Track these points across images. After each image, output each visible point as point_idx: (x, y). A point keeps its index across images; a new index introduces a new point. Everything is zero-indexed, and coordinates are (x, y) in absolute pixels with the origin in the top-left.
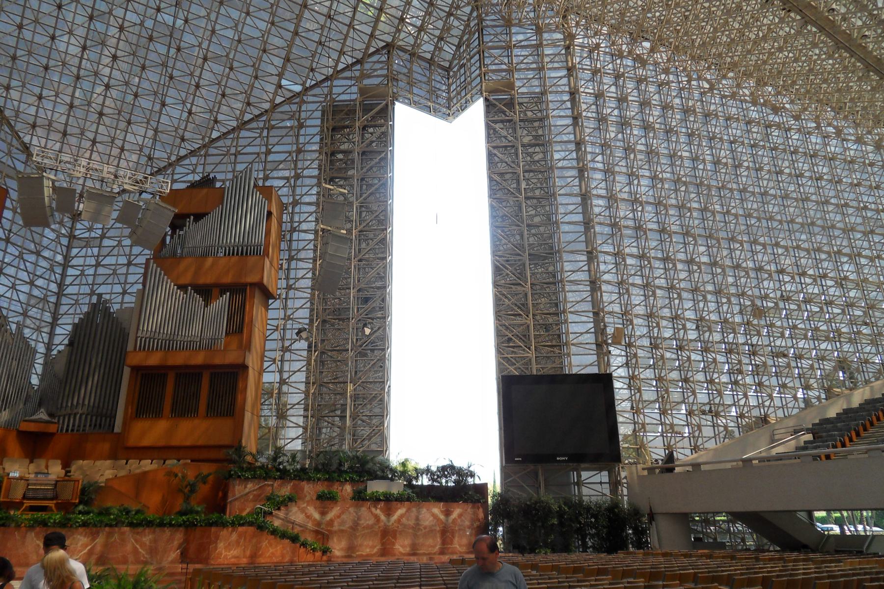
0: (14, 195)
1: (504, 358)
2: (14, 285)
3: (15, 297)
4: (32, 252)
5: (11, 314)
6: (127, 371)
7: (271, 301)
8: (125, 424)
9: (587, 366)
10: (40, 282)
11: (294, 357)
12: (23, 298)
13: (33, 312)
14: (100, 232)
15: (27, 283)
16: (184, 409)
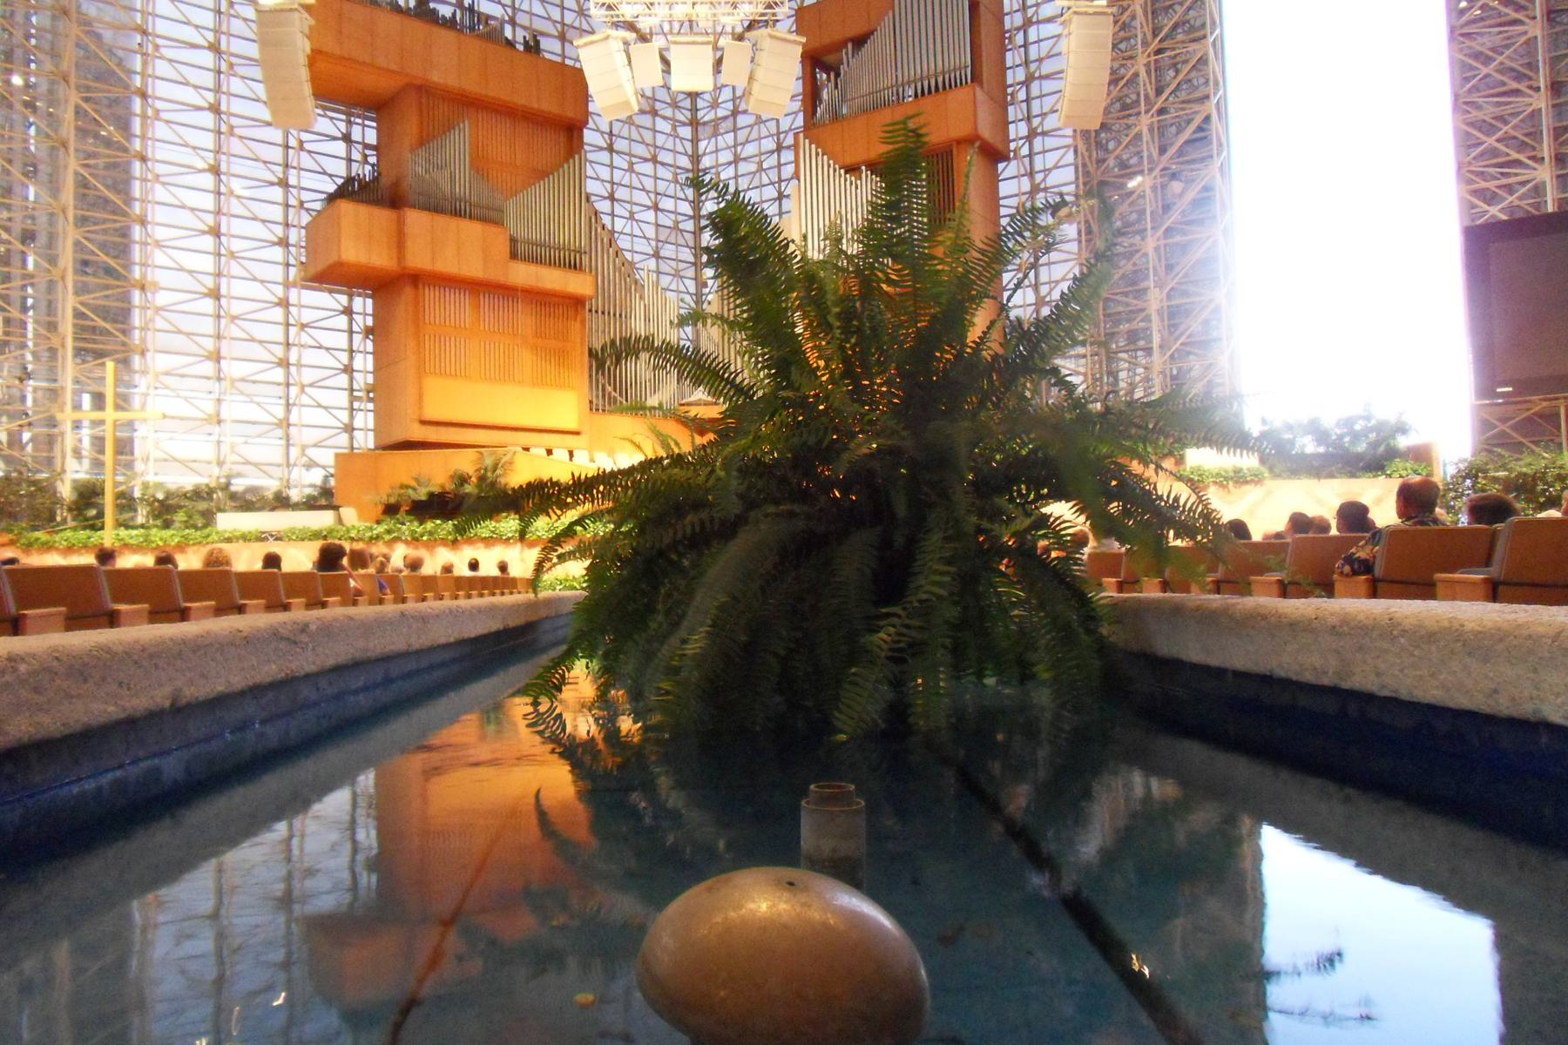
1: (1475, 192)
2: (632, 214)
3: (637, 232)
4: (646, 160)
5: (637, 258)
7: (1001, 166)
9: (248, 463)
10: (666, 204)
12: (650, 232)
13: (668, 251)
14: (730, 106)
15: (649, 208)
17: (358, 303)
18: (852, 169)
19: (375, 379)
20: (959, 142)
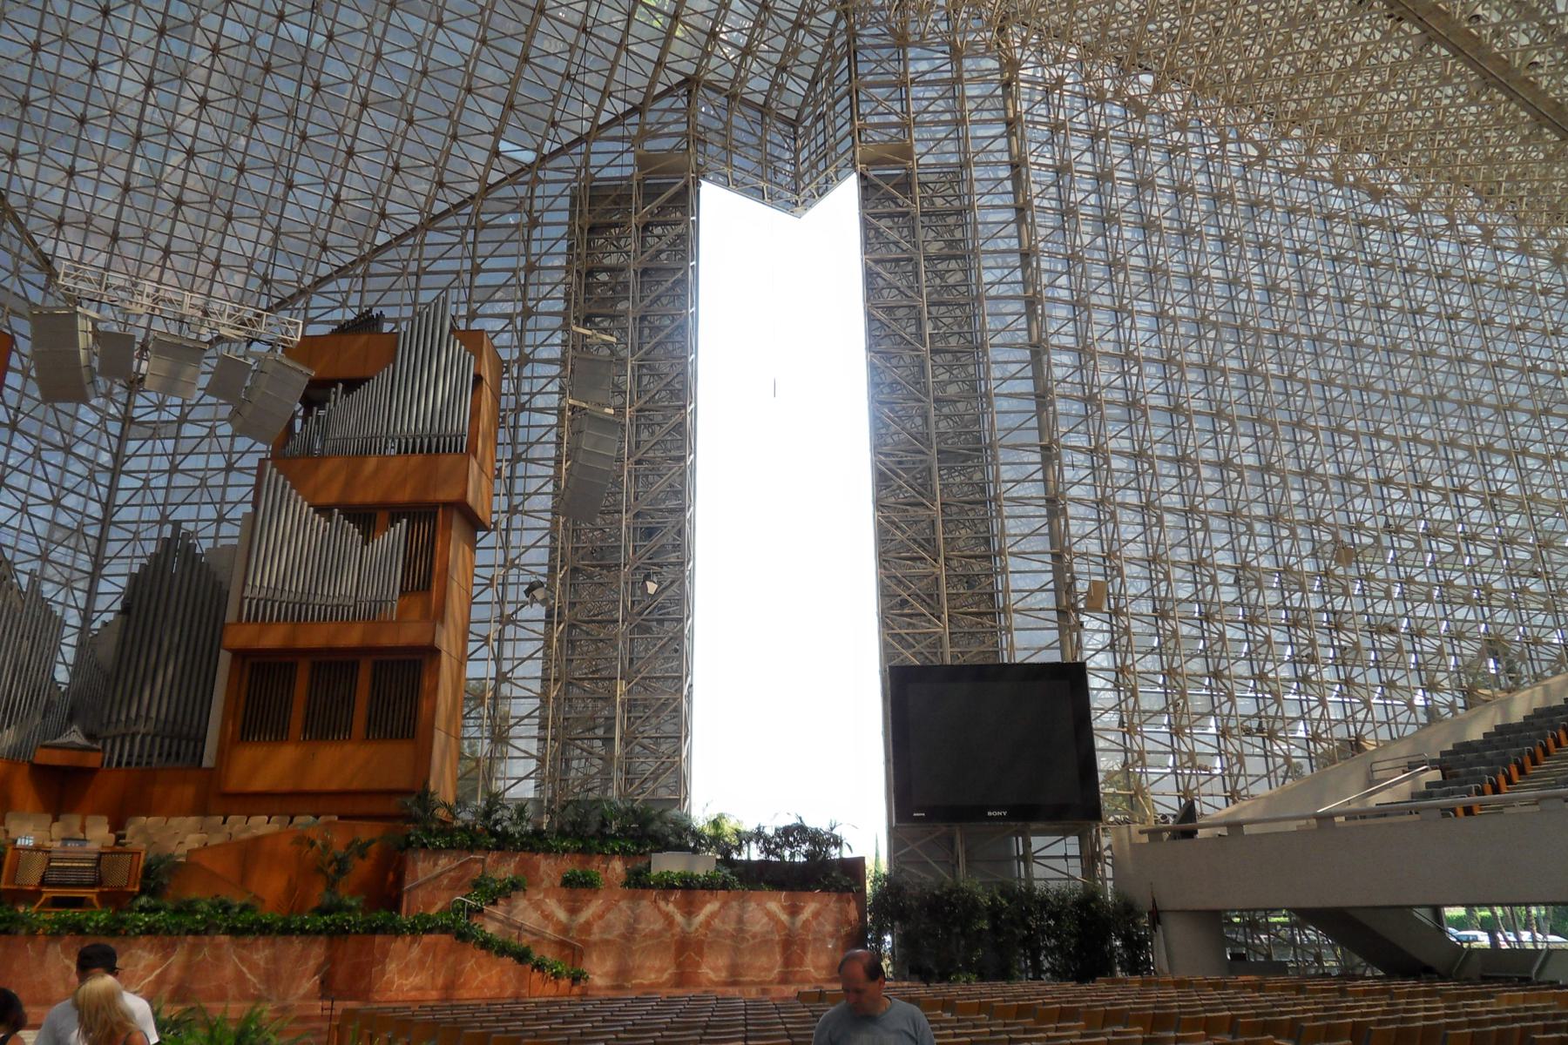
0: (24, 346)
2: (25, 505)
3: (27, 527)
4: (57, 448)
5: (19, 557)
6: (225, 658)
7: (480, 534)
8: (221, 752)
9: (1040, 649)
10: (71, 501)
11: (521, 633)
12: (41, 528)
13: (59, 554)
14: (177, 411)
15: (48, 502)
16: (326, 725)
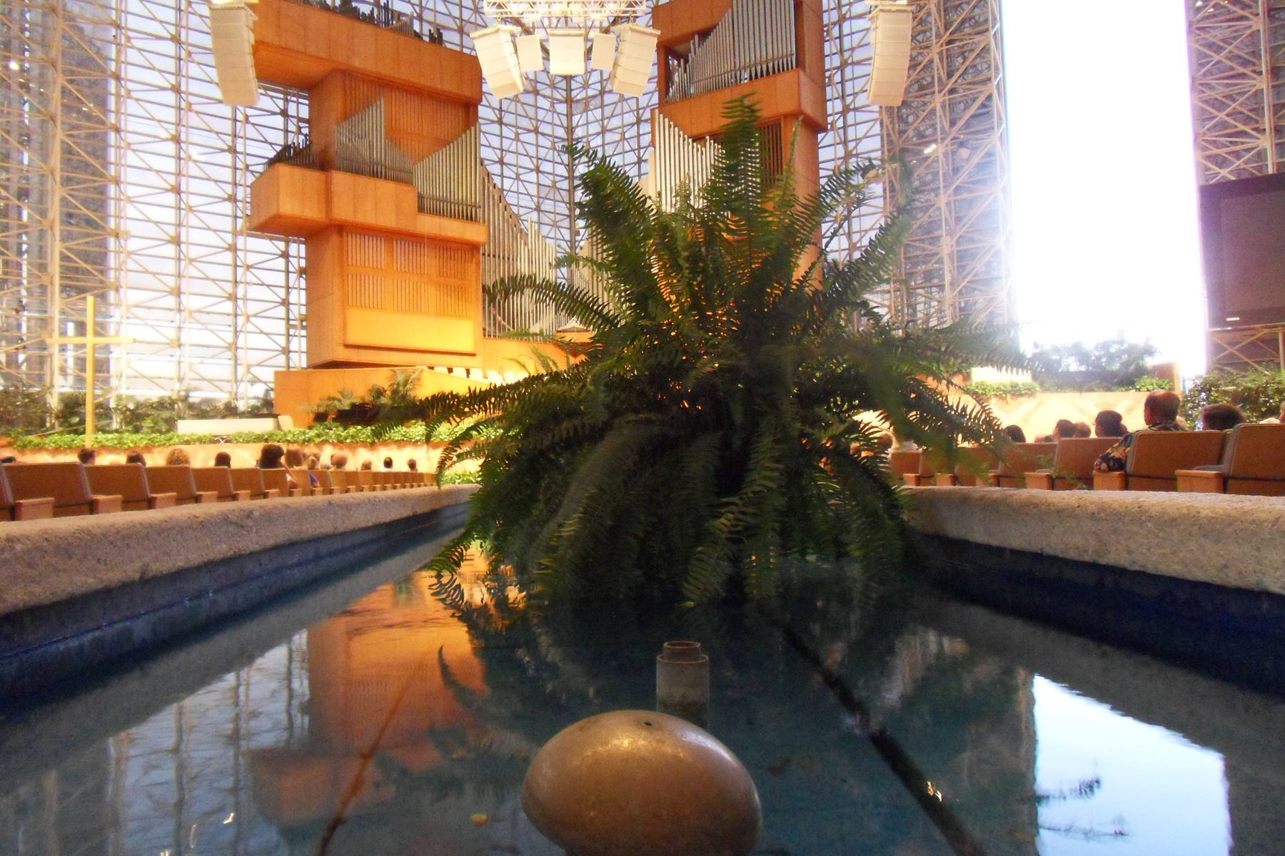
1: (1209, 158)
2: (518, 175)
3: (522, 190)
4: (529, 131)
5: (522, 211)
7: (820, 136)
9: (203, 379)
10: (546, 167)
12: (533, 190)
13: (547, 205)
14: (598, 86)
15: (532, 170)
17: (293, 248)
18: (698, 139)
19: (307, 310)
20: (786, 116)
